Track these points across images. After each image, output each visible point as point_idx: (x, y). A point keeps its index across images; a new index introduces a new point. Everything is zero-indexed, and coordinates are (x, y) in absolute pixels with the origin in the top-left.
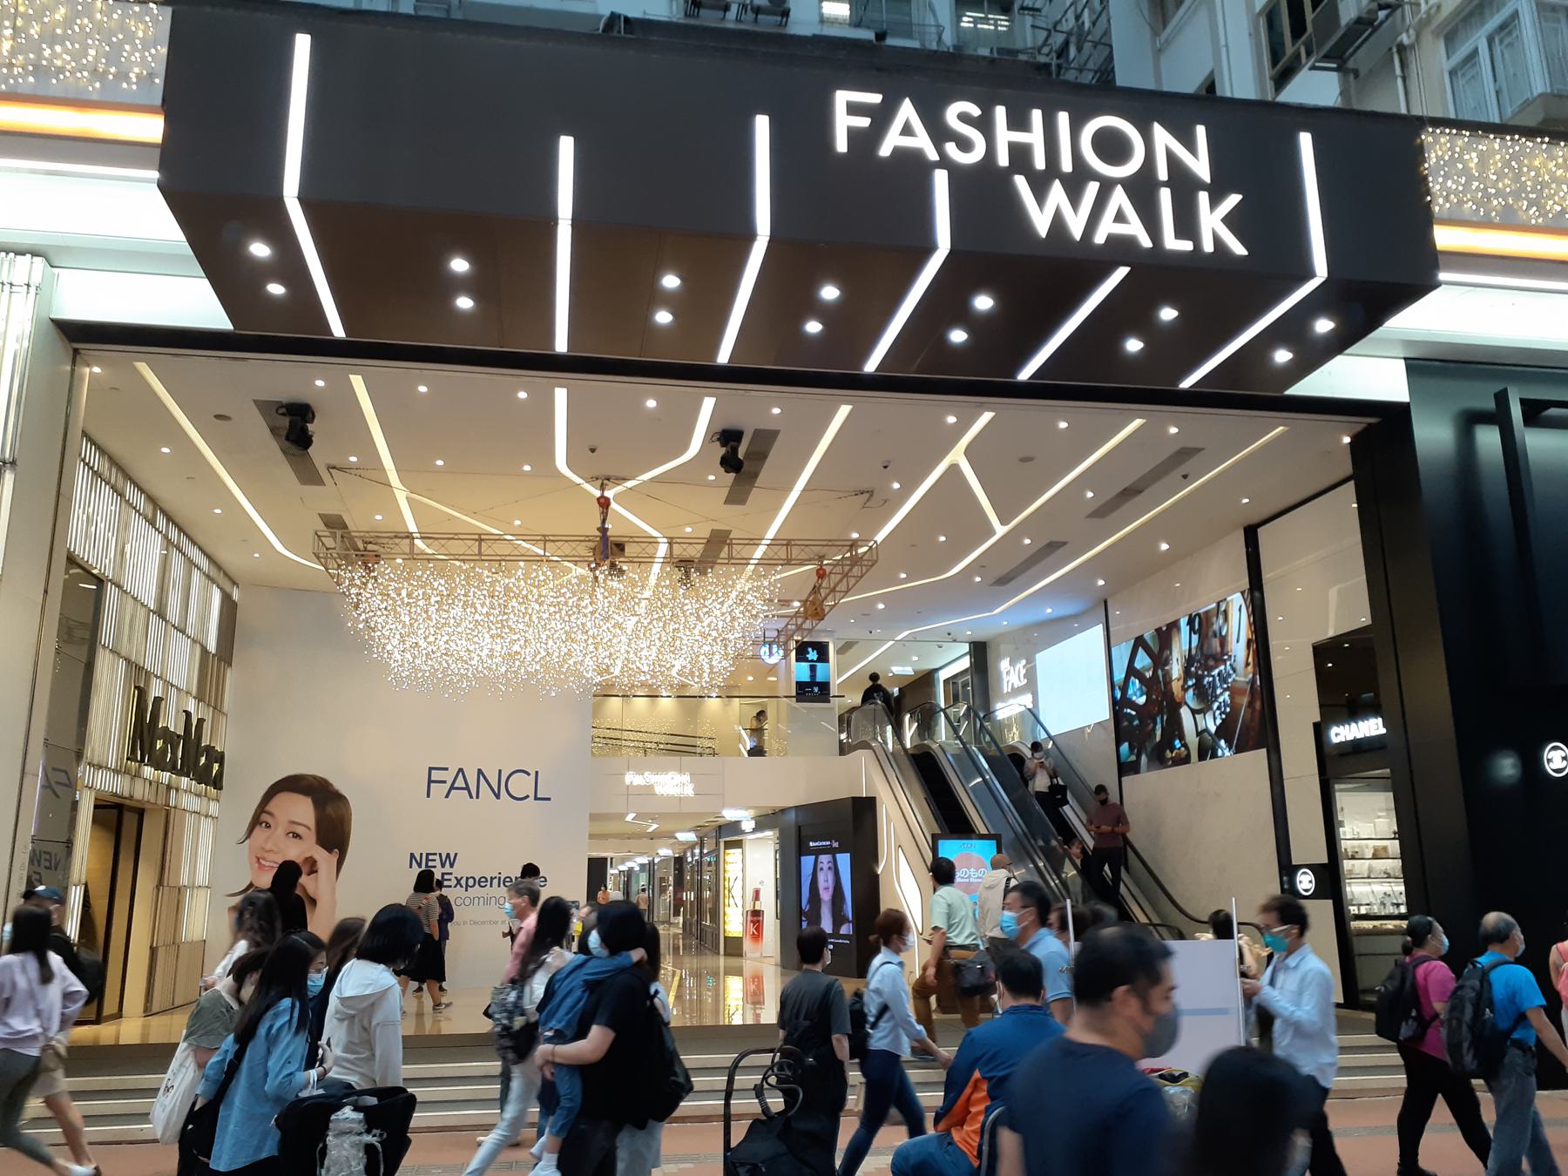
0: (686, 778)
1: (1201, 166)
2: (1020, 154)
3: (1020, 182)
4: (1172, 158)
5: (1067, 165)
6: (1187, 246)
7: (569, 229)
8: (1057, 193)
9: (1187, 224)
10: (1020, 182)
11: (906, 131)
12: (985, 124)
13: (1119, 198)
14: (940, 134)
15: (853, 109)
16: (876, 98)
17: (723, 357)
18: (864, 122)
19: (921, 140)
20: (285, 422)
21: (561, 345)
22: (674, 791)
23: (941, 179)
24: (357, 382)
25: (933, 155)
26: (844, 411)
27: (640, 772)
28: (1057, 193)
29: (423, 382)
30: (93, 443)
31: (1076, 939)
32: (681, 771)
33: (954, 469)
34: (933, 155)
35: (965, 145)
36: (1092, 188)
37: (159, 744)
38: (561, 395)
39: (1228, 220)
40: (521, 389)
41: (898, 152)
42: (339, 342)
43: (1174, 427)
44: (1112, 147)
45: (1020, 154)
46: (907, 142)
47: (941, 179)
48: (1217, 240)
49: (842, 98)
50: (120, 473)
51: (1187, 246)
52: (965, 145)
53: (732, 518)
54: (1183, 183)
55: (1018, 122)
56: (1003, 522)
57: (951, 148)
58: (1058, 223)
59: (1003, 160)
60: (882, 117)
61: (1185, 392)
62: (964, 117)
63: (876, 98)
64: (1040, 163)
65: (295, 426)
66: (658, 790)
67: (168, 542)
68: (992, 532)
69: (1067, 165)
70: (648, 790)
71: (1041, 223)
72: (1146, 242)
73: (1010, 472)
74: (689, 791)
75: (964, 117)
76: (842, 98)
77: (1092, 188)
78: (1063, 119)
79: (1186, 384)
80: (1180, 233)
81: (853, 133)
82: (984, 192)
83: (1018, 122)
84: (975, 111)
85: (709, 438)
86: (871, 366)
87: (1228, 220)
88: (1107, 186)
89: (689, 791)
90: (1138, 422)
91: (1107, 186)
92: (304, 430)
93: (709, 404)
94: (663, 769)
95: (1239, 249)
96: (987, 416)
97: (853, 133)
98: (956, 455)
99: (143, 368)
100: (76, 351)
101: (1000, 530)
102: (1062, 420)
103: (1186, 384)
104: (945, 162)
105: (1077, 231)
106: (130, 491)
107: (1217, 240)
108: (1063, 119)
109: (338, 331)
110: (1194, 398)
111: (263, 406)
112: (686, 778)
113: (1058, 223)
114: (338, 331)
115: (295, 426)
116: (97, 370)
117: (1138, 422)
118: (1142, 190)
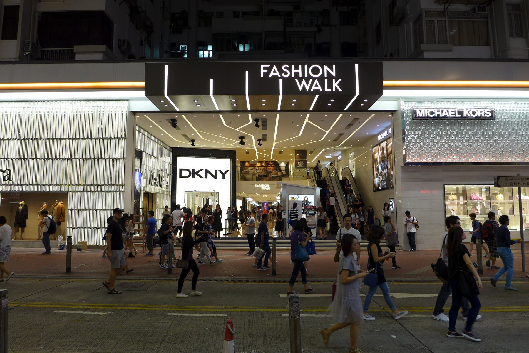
0: (268, 186)
1: (334, 74)
2: (297, 74)
3: (296, 80)
4: (307, 84)
5: (306, 76)
6: (330, 90)
8: (304, 82)
9: (330, 86)
10: (296, 80)
11: (274, 72)
12: (290, 69)
13: (316, 81)
14: (281, 71)
16: (269, 66)
18: (266, 71)
19: (277, 74)
23: (281, 80)
25: (279, 76)
28: (304, 82)
32: (267, 184)
34: (279, 76)
36: (311, 80)
39: (338, 84)
45: (297, 74)
47: (281, 80)
49: (262, 66)
51: (330, 90)
55: (297, 68)
57: (283, 74)
58: (304, 87)
59: (293, 76)
60: (269, 70)
62: (286, 68)
63: (269, 66)
64: (301, 76)
66: (263, 188)
69: (306, 76)
70: (260, 188)
71: (300, 88)
72: (321, 90)
74: (269, 188)
75: (286, 68)
76: (262, 66)
77: (311, 80)
78: (306, 66)
81: (264, 73)
82: (290, 83)
83: (297, 68)
84: (288, 66)
88: (314, 79)
89: (269, 188)
91: (314, 79)
95: (340, 90)
97: (264, 73)
104: (282, 77)
105: (307, 88)
108: (306, 66)
112: (268, 186)
113: (304, 87)
118: (321, 80)
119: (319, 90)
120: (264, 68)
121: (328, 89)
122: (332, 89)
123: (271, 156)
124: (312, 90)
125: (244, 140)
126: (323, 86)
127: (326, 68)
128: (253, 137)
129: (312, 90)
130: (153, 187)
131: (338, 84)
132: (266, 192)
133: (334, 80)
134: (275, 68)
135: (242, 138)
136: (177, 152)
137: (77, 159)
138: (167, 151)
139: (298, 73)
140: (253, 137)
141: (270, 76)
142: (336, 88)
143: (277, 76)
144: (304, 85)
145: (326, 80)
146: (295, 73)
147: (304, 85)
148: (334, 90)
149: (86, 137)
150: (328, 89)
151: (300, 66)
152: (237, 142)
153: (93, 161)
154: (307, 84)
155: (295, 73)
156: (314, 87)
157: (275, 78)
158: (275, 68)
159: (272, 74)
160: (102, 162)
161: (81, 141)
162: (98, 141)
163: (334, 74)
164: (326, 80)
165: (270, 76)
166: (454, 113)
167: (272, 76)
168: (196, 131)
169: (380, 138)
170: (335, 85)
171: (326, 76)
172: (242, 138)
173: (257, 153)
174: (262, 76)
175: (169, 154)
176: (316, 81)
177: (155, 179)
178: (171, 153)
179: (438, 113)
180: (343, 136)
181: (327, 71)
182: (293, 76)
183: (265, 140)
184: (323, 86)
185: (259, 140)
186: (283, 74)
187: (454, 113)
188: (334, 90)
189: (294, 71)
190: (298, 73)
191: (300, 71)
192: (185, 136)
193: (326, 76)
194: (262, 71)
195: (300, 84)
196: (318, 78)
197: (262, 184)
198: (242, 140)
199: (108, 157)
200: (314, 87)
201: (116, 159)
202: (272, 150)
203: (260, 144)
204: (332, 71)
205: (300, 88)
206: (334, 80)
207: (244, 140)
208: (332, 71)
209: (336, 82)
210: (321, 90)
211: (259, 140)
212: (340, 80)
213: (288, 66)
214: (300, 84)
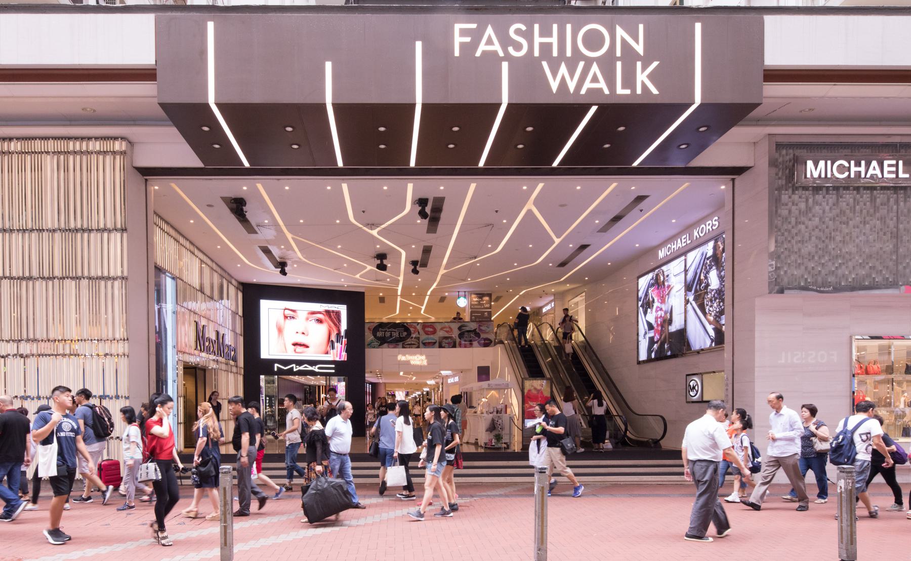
0: (424, 357)
1: (640, 48)
2: (546, 49)
3: (545, 64)
4: (572, 77)
5: (569, 54)
6: (628, 92)
7: (821, 94)
8: (563, 70)
9: (629, 80)
10: (545, 64)
11: (489, 43)
12: (528, 35)
13: (595, 68)
14: (506, 41)
15: (890, 166)
16: (474, 26)
17: (481, 164)
19: (497, 47)
20: (234, 206)
21: (412, 164)
22: (418, 363)
23: (505, 65)
24: (259, 186)
25: (501, 54)
26: (473, 186)
27: (404, 355)
28: (563, 70)
29: (288, 184)
30: (159, 216)
31: (29, 421)
32: (421, 354)
33: (530, 212)
34: (501, 54)
35: (518, 47)
36: (581, 64)
37: (207, 344)
38: (345, 187)
39: (649, 77)
40: (328, 184)
41: (484, 53)
42: (247, 169)
43: (635, 185)
44: (593, 41)
45: (546, 49)
46: (490, 48)
47: (505, 65)
48: (644, 86)
49: (458, 27)
50: (178, 233)
51: (628, 92)
52: (518, 47)
53: (430, 239)
54: (629, 55)
56: (558, 237)
57: (511, 49)
58: (563, 82)
59: (537, 53)
60: (476, 36)
61: (635, 168)
62: (518, 32)
63: (474, 26)
65: (238, 206)
66: (412, 363)
67: (202, 261)
68: (554, 242)
69: (569, 54)
70: (407, 363)
71: (554, 85)
72: (607, 92)
73: (559, 211)
74: (425, 363)
75: (518, 32)
76: (458, 27)
77: (581, 64)
78: (569, 27)
79: (635, 164)
80: (624, 87)
81: (462, 45)
83: (545, 32)
84: (523, 28)
85: (414, 203)
86: (481, 164)
87: (651, 77)
88: (589, 62)
89: (425, 363)
90: (614, 185)
91: (589, 62)
92: (242, 210)
93: (410, 187)
94: (415, 354)
95: (655, 91)
96: (541, 185)
97: (462, 45)
98: (530, 205)
99: (173, 185)
100: (146, 180)
101: (557, 241)
102: (578, 184)
103: (635, 164)
104: (508, 57)
105: (572, 86)
106: (182, 240)
107: (644, 86)
109: (246, 164)
110: (640, 171)
111: (224, 199)
112: (424, 357)
113: (563, 82)
114: (246, 164)
115: (238, 206)
116: (156, 188)
117: (614, 185)
119: (601, 90)
120: (463, 33)
121: (623, 87)
122: (634, 89)
123: (423, 308)
124: (583, 92)
125: (385, 262)
126: (611, 83)
127: (620, 32)
128: (404, 254)
129: (583, 92)
130: (204, 354)
131: (649, 77)
132: (419, 371)
133: (639, 64)
134: (490, 31)
135: (381, 257)
136: (253, 294)
137: (11, 278)
138: (232, 290)
139: (550, 45)
140: (404, 254)
141: (478, 54)
142: (643, 84)
143: (495, 53)
144: (563, 78)
145: (619, 64)
146: (542, 45)
147: (563, 78)
148: (639, 91)
149: (30, 226)
150: (623, 87)
151: (555, 26)
152: (369, 268)
153: (50, 283)
154: (572, 77)
155: (542, 45)
156: (588, 85)
157: (491, 59)
158: (490, 31)
159: (483, 47)
160: (70, 285)
161: (17, 238)
162: (57, 235)
163: (640, 48)
164: (619, 64)
165: (478, 54)
166: (894, 169)
167: (484, 52)
168: (289, 236)
169: (661, 254)
170: (642, 77)
171: (618, 54)
172: (381, 257)
173: (399, 299)
174: (457, 54)
175: (237, 295)
176: (595, 68)
177: (209, 340)
178: (240, 295)
179: (858, 169)
180: (588, 248)
181: (624, 42)
182: (537, 53)
183: (424, 265)
184: (611, 83)
185: (415, 263)
186: (511, 49)
187: (894, 169)
188: (639, 91)
189: (538, 40)
190: (550, 45)
191: (554, 40)
192: (267, 251)
193: (618, 54)
194: (458, 40)
195: (554, 75)
196: (598, 60)
197: (411, 354)
198: (382, 262)
199: (86, 274)
200: (588, 85)
201: (102, 278)
202: (429, 293)
203: (415, 272)
204: (637, 41)
205: (554, 85)
206: (639, 64)
207: (385, 262)
208: (637, 41)
209: (644, 69)
210: (607, 92)
211: (415, 263)
212: (655, 64)
213: (523, 28)
214: (554, 75)
